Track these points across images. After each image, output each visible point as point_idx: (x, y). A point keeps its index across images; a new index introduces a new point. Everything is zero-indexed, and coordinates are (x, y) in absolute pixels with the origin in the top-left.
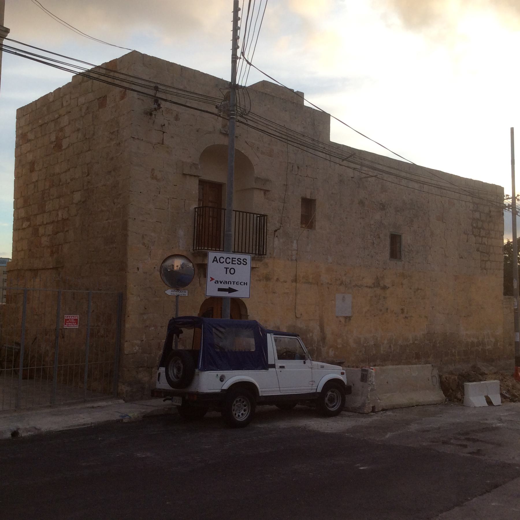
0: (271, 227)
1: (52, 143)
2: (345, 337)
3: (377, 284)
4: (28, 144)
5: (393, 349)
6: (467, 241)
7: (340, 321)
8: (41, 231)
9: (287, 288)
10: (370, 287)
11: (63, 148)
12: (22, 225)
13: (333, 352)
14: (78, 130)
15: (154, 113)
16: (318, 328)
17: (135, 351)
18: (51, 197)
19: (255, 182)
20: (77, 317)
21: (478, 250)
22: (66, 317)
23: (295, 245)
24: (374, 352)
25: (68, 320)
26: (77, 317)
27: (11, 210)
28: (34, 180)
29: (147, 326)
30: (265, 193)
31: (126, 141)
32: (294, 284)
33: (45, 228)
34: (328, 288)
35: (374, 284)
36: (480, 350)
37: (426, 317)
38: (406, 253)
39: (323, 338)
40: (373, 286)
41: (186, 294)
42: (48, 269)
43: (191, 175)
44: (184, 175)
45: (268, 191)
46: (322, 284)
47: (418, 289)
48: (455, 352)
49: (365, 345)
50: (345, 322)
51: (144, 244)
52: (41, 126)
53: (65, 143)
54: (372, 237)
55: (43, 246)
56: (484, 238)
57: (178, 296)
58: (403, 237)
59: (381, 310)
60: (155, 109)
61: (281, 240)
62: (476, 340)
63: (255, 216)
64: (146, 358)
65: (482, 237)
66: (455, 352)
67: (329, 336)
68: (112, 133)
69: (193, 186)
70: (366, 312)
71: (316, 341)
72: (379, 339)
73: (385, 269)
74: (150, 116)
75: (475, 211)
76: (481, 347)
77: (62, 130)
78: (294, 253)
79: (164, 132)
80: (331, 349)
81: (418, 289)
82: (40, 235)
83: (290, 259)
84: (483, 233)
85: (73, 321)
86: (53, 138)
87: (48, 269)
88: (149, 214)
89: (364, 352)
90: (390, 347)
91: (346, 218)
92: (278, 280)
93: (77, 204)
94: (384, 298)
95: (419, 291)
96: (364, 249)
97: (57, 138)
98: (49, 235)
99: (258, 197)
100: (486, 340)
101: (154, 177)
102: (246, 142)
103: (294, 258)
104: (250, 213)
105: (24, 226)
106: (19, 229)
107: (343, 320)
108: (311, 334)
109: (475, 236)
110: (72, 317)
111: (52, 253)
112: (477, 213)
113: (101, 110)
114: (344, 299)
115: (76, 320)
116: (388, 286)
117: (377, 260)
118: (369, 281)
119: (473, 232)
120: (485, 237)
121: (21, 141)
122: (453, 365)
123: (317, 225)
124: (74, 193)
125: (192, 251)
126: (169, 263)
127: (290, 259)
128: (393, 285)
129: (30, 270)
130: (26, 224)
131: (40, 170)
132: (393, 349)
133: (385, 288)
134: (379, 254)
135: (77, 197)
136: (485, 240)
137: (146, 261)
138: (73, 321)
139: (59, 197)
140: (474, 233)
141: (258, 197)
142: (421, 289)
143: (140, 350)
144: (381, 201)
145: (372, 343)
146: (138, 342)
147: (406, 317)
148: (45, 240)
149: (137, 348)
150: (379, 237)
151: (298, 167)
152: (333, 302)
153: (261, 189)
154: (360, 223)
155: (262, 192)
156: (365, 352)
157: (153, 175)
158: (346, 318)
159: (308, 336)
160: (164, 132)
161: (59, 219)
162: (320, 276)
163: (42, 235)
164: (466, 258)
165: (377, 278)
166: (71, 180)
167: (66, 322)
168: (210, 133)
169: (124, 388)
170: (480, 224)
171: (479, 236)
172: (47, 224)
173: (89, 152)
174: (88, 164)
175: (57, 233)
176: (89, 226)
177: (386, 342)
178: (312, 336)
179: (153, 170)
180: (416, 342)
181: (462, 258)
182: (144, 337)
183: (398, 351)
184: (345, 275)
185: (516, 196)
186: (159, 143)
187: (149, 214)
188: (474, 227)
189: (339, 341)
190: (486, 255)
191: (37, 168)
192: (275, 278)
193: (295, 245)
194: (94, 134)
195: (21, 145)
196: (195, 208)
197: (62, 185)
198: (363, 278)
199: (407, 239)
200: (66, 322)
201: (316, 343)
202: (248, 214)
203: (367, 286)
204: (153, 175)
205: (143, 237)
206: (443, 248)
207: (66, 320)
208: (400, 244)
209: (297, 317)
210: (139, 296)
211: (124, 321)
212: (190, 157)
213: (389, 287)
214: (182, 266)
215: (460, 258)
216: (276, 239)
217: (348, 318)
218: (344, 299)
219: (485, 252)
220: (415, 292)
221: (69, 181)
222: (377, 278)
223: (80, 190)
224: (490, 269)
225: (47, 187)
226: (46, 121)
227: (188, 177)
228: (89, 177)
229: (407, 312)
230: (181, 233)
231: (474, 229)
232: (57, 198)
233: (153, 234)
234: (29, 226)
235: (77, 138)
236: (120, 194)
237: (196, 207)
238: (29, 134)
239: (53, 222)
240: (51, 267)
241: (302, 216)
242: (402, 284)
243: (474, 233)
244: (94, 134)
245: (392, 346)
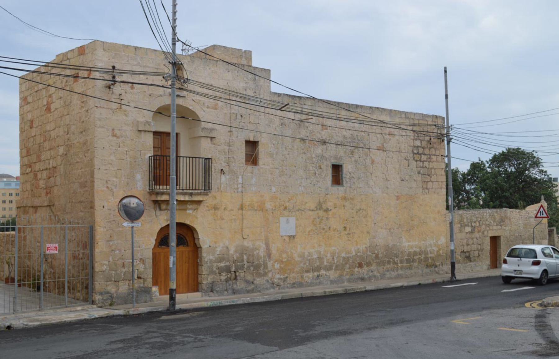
0: (216, 167)
1: (44, 106)
2: (290, 253)
3: (320, 206)
4: (28, 106)
5: (336, 261)
6: (408, 166)
7: (285, 240)
8: (39, 176)
9: (234, 215)
10: (313, 210)
11: (52, 110)
12: (26, 171)
13: (278, 265)
14: (61, 98)
15: (112, 86)
16: (264, 246)
17: (104, 269)
18: (45, 149)
19: (202, 132)
20: (57, 245)
21: (419, 173)
22: (48, 245)
23: (240, 180)
24: (318, 264)
25: (49, 247)
26: (57, 245)
27: (18, 158)
28: (33, 135)
29: (113, 250)
30: (211, 140)
31: (91, 109)
32: (240, 212)
33: (42, 173)
34: (272, 213)
35: (316, 207)
36: (422, 258)
37: (368, 233)
38: (348, 180)
39: (269, 255)
40: (316, 209)
41: (140, 225)
42: (44, 206)
43: (145, 131)
44: (140, 131)
45: (214, 138)
46: (267, 210)
47: (360, 210)
48: (397, 261)
49: (309, 258)
50: (290, 240)
51: (107, 187)
52: (37, 91)
53: (53, 107)
54: (314, 168)
55: (41, 187)
56: (425, 163)
57: (132, 227)
58: (344, 166)
59: (324, 229)
60: (112, 84)
61: (228, 177)
62: (418, 250)
63: (203, 159)
64: (113, 275)
65: (423, 162)
66: (397, 261)
67: (274, 252)
68: (83, 102)
69: (149, 140)
70: (309, 232)
71: (262, 256)
72: (322, 253)
73: (327, 194)
74: (109, 89)
75: (416, 140)
76: (423, 256)
77: (50, 96)
78: (240, 186)
79: (121, 100)
80: (277, 263)
81: (360, 210)
82: (38, 179)
83: (236, 192)
84: (424, 158)
85: (53, 248)
86: (45, 103)
87: (44, 206)
88: (111, 164)
89: (308, 264)
90: (333, 259)
91: (288, 154)
92: (225, 209)
93: (61, 156)
94: (327, 219)
95: (361, 211)
96: (306, 179)
97: (48, 102)
98: (44, 179)
99: (205, 144)
100: (428, 250)
101: (114, 135)
102: (193, 100)
103: (240, 190)
104: (199, 158)
105: (27, 171)
106: (24, 174)
107: (287, 239)
108: (257, 251)
109: (416, 161)
110: (52, 245)
111: (47, 193)
112: (418, 141)
113: (75, 84)
114: (288, 222)
115: (56, 247)
116: (330, 208)
117: (320, 187)
118: (312, 205)
119: (414, 158)
120: (426, 161)
121: (23, 103)
122: (395, 271)
123: (261, 162)
124: (59, 147)
125: (148, 190)
126: (125, 201)
127: (236, 192)
128: (335, 208)
129: (32, 207)
130: (29, 170)
131: (37, 127)
132: (336, 261)
133: (327, 210)
134: (321, 183)
135: (61, 150)
136: (426, 164)
137: (110, 200)
138: (53, 248)
139: (50, 149)
140: (415, 159)
141: (205, 144)
142: (363, 209)
143: (108, 269)
144: (322, 137)
145: (315, 256)
146: (107, 263)
147: (349, 234)
148: (42, 184)
149: (106, 267)
150: (321, 168)
151: (241, 116)
152: (278, 224)
153: (207, 137)
154: (302, 158)
155: (209, 139)
156: (309, 264)
157: (113, 133)
158: (290, 237)
159: (255, 253)
160: (121, 100)
161: (51, 167)
162: (264, 204)
163: (40, 179)
164: (407, 181)
165: (320, 202)
166: (57, 137)
167: (48, 249)
168: (161, 96)
169: (97, 297)
170: (421, 150)
171: (420, 161)
172: (43, 170)
173: (68, 116)
174: (67, 125)
175: (50, 178)
176: (69, 173)
177: (329, 255)
178: (259, 253)
179: (113, 130)
180: (359, 254)
181: (403, 180)
182: (111, 259)
183: (341, 262)
184: (288, 201)
185: (450, 125)
186: (117, 109)
187: (111, 164)
188: (415, 154)
189: (284, 256)
190: (427, 176)
191: (34, 126)
192: (223, 208)
193: (240, 180)
194: (71, 102)
195: (23, 106)
196: (150, 157)
197: (52, 140)
198: (306, 203)
199: (347, 168)
200: (48, 249)
201: (262, 258)
202: (194, 159)
203: (310, 210)
204: (113, 133)
205: (107, 182)
206: (383, 173)
207: (48, 248)
208: (342, 173)
209: (244, 238)
210: (105, 227)
211: (94, 247)
212: (144, 117)
213: (331, 210)
214: (137, 203)
215: (401, 180)
216: (223, 176)
217: (292, 237)
218: (288, 222)
219: (426, 174)
220: (357, 212)
221: (56, 137)
222: (320, 202)
223: (63, 145)
224: (432, 188)
225: (42, 141)
226: (40, 89)
227: (143, 133)
228: (68, 135)
229: (350, 229)
230: (138, 177)
231: (415, 156)
232: (49, 150)
233: (114, 179)
234: (31, 171)
235: (60, 104)
236: (89, 150)
237: (150, 155)
238: (28, 98)
239: (46, 169)
240: (46, 205)
241: (246, 154)
242: (344, 206)
243: (415, 159)
244: (71, 102)
245: (335, 258)
